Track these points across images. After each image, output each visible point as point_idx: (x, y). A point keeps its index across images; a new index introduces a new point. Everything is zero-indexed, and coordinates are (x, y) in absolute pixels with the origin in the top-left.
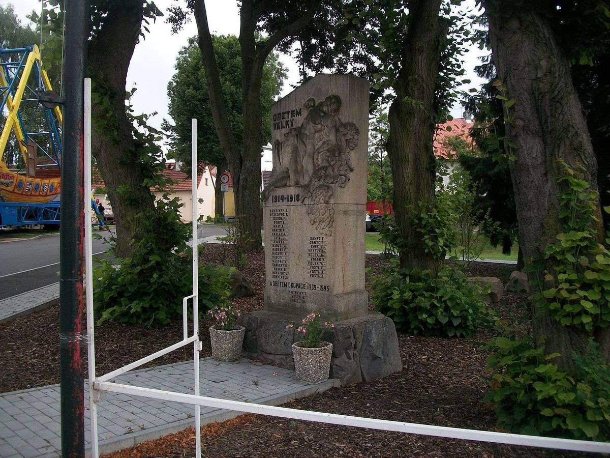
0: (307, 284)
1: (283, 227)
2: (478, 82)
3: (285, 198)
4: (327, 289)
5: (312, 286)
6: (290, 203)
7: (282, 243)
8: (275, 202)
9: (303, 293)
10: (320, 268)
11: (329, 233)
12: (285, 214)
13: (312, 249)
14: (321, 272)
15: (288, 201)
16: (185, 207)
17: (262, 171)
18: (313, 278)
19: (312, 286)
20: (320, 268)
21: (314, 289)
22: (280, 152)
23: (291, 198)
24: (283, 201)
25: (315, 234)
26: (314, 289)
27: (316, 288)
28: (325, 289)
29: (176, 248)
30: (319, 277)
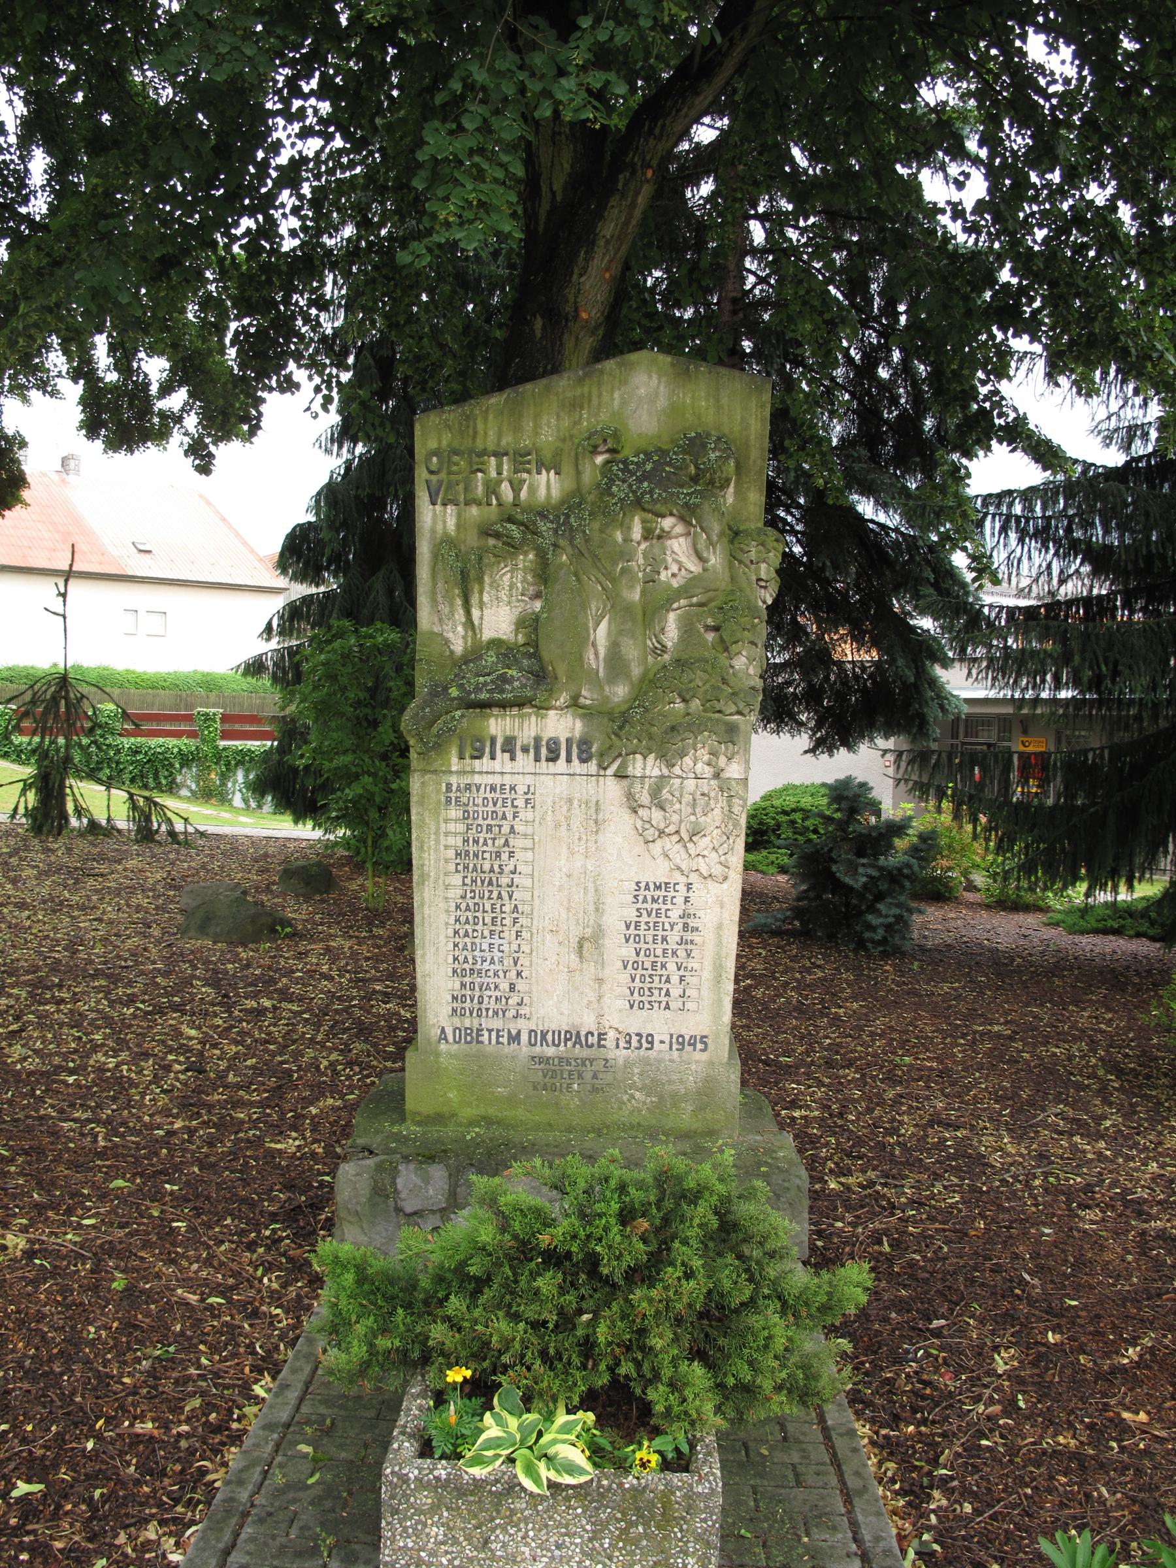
0: (612, 1035)
1: (506, 843)
2: (860, 509)
3: (525, 750)
4: (699, 1046)
5: (635, 1039)
6: (552, 767)
7: (500, 897)
8: (548, 760)
9: (591, 1061)
10: (675, 979)
11: (718, 870)
12: (520, 803)
13: (645, 918)
14: (675, 992)
15: (537, 759)
16: (261, 635)
17: (971, 491)
18: (644, 1013)
19: (635, 1039)
20: (675, 979)
21: (645, 1045)
22: (474, 600)
23: (550, 750)
24: (513, 759)
25: (658, 872)
26: (645, 1045)
27: (652, 1043)
28: (694, 1045)
29: (299, 322)
30: (667, 1007)
